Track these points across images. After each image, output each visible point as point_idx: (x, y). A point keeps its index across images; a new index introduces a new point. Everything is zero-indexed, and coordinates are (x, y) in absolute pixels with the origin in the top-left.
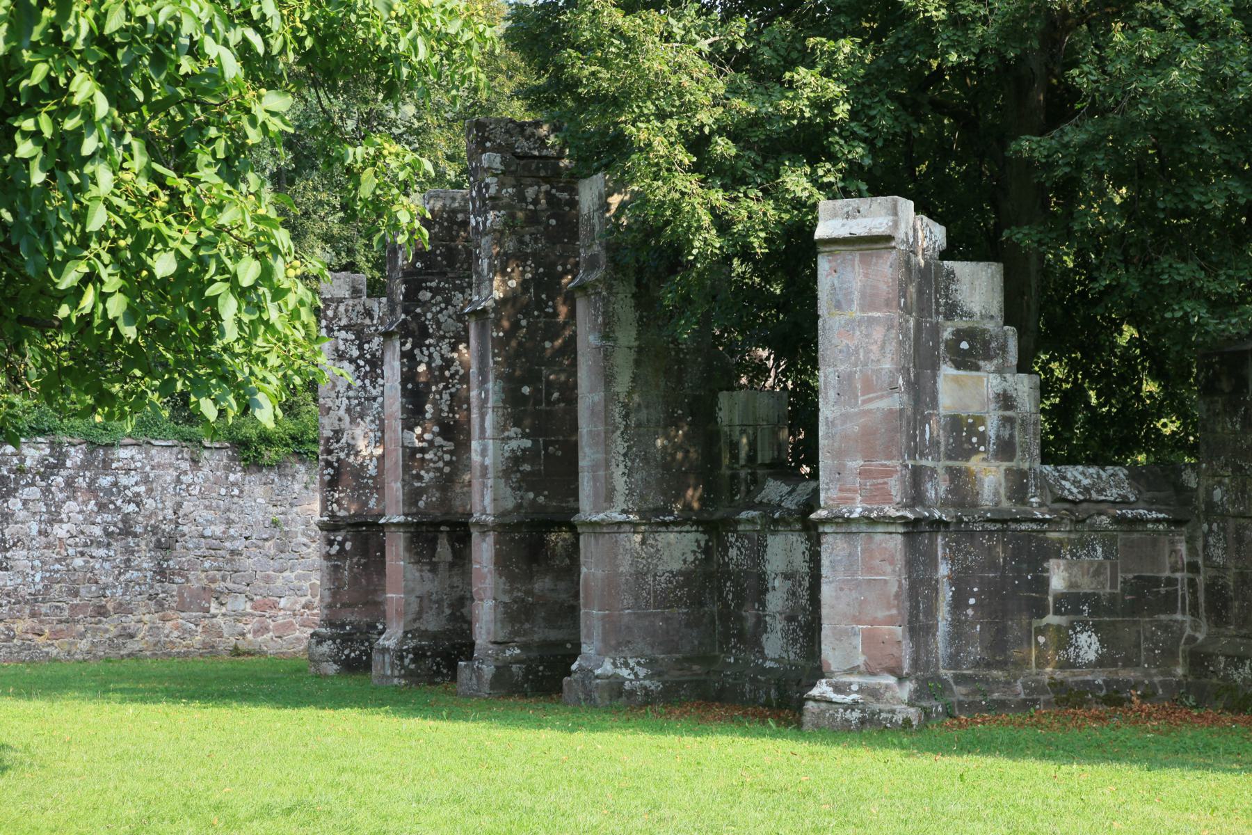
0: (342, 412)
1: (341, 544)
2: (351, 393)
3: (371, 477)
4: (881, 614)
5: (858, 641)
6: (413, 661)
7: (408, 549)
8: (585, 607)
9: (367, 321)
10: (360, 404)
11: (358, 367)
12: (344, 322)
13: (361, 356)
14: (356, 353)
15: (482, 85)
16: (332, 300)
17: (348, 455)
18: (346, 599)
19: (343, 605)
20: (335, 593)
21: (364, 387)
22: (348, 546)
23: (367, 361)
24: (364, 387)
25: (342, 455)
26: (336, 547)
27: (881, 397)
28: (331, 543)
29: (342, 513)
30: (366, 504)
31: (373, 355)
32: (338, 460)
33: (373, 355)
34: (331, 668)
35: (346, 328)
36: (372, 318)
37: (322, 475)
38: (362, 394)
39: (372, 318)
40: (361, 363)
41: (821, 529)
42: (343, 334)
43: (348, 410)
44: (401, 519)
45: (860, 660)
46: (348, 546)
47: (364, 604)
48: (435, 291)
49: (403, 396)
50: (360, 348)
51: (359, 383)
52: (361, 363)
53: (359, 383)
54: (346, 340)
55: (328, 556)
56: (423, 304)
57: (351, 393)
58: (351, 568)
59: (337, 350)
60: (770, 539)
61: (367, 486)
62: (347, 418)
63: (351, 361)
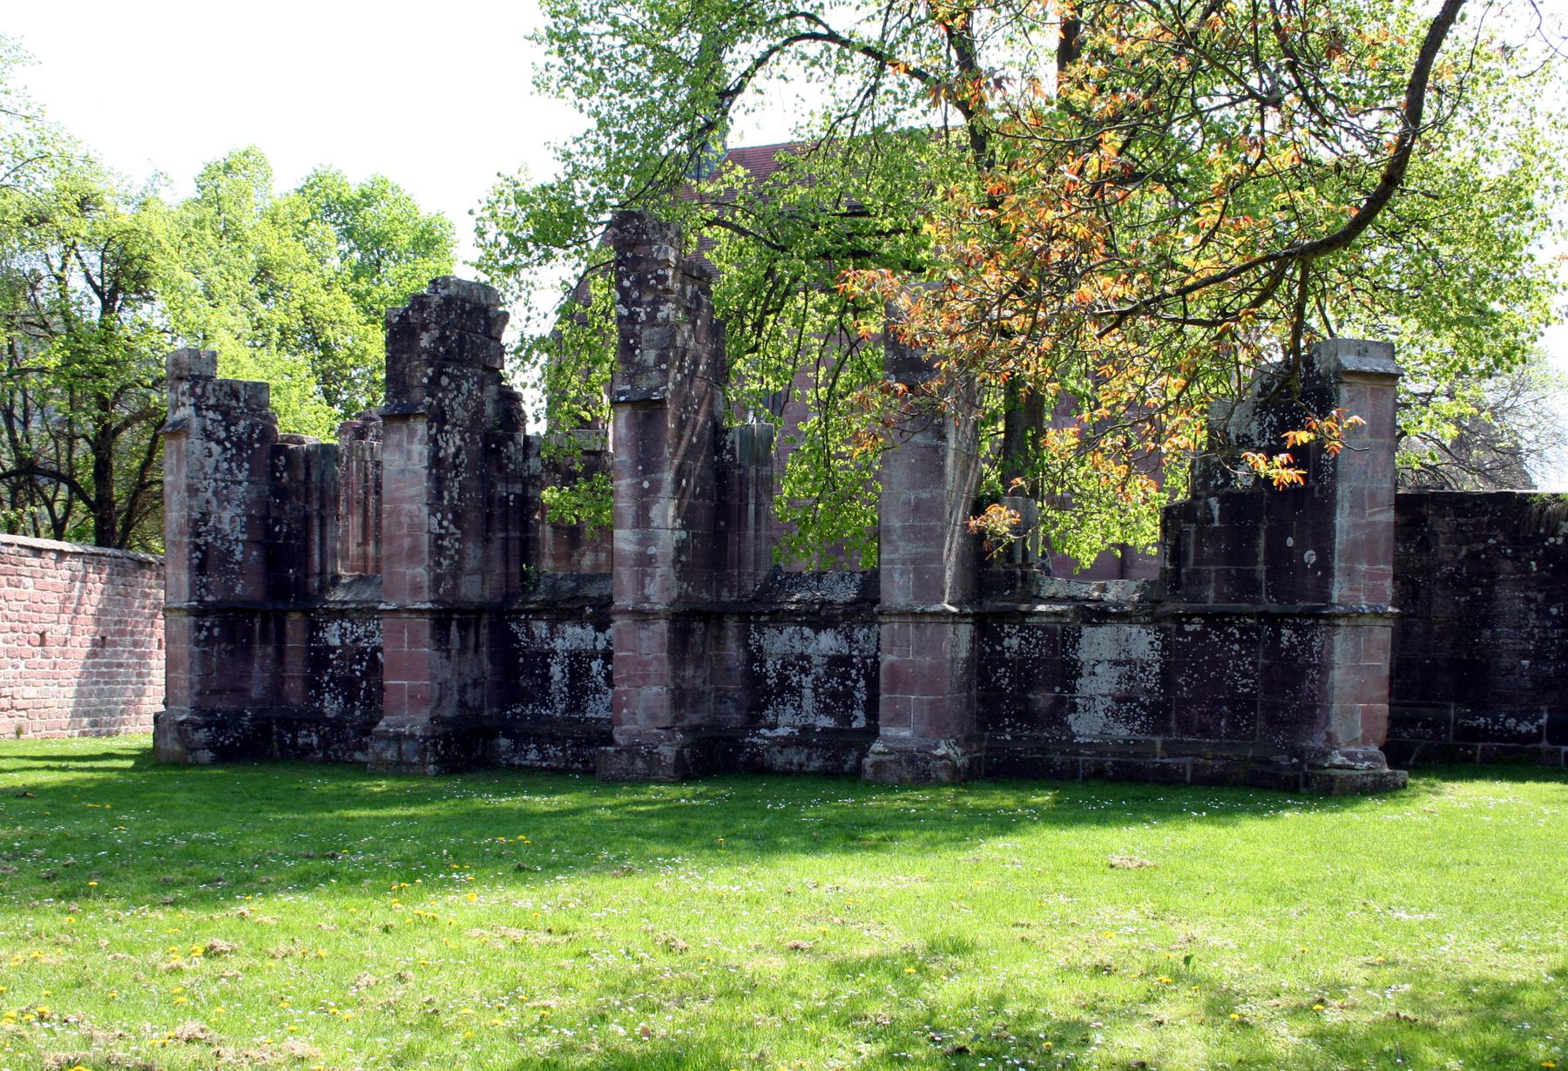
0: (209, 494)
1: (210, 629)
2: (218, 476)
3: (237, 563)
4: (1376, 694)
5: (1358, 717)
6: (443, 747)
7: (432, 636)
8: (888, 691)
9: (234, 403)
10: (226, 487)
11: (225, 449)
12: (212, 401)
13: (228, 438)
14: (223, 435)
15: (998, 159)
16: (199, 377)
17: (215, 539)
18: (214, 685)
19: (212, 692)
20: (206, 676)
21: (230, 470)
22: (216, 631)
23: (232, 442)
24: (230, 470)
25: (210, 539)
26: (205, 633)
27: (1381, 512)
28: (199, 628)
29: (209, 598)
30: (232, 589)
31: (239, 438)
32: (206, 543)
33: (239, 438)
34: (206, 755)
35: (215, 408)
36: (238, 400)
37: (190, 559)
38: (228, 477)
39: (238, 400)
40: (228, 445)
41: (1337, 622)
42: (211, 414)
43: (215, 493)
44: (429, 605)
45: (1359, 733)
46: (216, 631)
47: (232, 690)
48: (452, 378)
49: (429, 480)
50: (227, 429)
51: (225, 465)
52: (228, 445)
53: (225, 465)
54: (214, 421)
55: (197, 643)
56: (444, 389)
57: (218, 476)
58: (219, 654)
59: (204, 429)
60: (1086, 630)
61: (233, 571)
62: (214, 501)
63: (219, 442)
